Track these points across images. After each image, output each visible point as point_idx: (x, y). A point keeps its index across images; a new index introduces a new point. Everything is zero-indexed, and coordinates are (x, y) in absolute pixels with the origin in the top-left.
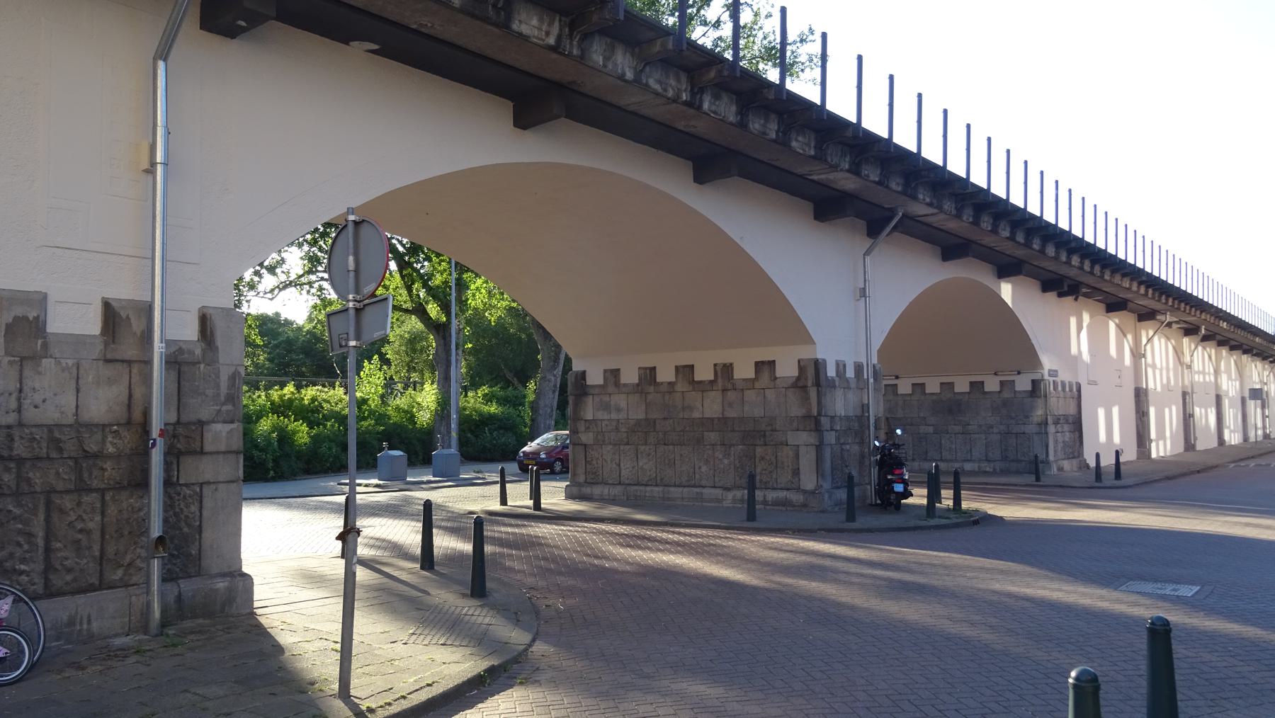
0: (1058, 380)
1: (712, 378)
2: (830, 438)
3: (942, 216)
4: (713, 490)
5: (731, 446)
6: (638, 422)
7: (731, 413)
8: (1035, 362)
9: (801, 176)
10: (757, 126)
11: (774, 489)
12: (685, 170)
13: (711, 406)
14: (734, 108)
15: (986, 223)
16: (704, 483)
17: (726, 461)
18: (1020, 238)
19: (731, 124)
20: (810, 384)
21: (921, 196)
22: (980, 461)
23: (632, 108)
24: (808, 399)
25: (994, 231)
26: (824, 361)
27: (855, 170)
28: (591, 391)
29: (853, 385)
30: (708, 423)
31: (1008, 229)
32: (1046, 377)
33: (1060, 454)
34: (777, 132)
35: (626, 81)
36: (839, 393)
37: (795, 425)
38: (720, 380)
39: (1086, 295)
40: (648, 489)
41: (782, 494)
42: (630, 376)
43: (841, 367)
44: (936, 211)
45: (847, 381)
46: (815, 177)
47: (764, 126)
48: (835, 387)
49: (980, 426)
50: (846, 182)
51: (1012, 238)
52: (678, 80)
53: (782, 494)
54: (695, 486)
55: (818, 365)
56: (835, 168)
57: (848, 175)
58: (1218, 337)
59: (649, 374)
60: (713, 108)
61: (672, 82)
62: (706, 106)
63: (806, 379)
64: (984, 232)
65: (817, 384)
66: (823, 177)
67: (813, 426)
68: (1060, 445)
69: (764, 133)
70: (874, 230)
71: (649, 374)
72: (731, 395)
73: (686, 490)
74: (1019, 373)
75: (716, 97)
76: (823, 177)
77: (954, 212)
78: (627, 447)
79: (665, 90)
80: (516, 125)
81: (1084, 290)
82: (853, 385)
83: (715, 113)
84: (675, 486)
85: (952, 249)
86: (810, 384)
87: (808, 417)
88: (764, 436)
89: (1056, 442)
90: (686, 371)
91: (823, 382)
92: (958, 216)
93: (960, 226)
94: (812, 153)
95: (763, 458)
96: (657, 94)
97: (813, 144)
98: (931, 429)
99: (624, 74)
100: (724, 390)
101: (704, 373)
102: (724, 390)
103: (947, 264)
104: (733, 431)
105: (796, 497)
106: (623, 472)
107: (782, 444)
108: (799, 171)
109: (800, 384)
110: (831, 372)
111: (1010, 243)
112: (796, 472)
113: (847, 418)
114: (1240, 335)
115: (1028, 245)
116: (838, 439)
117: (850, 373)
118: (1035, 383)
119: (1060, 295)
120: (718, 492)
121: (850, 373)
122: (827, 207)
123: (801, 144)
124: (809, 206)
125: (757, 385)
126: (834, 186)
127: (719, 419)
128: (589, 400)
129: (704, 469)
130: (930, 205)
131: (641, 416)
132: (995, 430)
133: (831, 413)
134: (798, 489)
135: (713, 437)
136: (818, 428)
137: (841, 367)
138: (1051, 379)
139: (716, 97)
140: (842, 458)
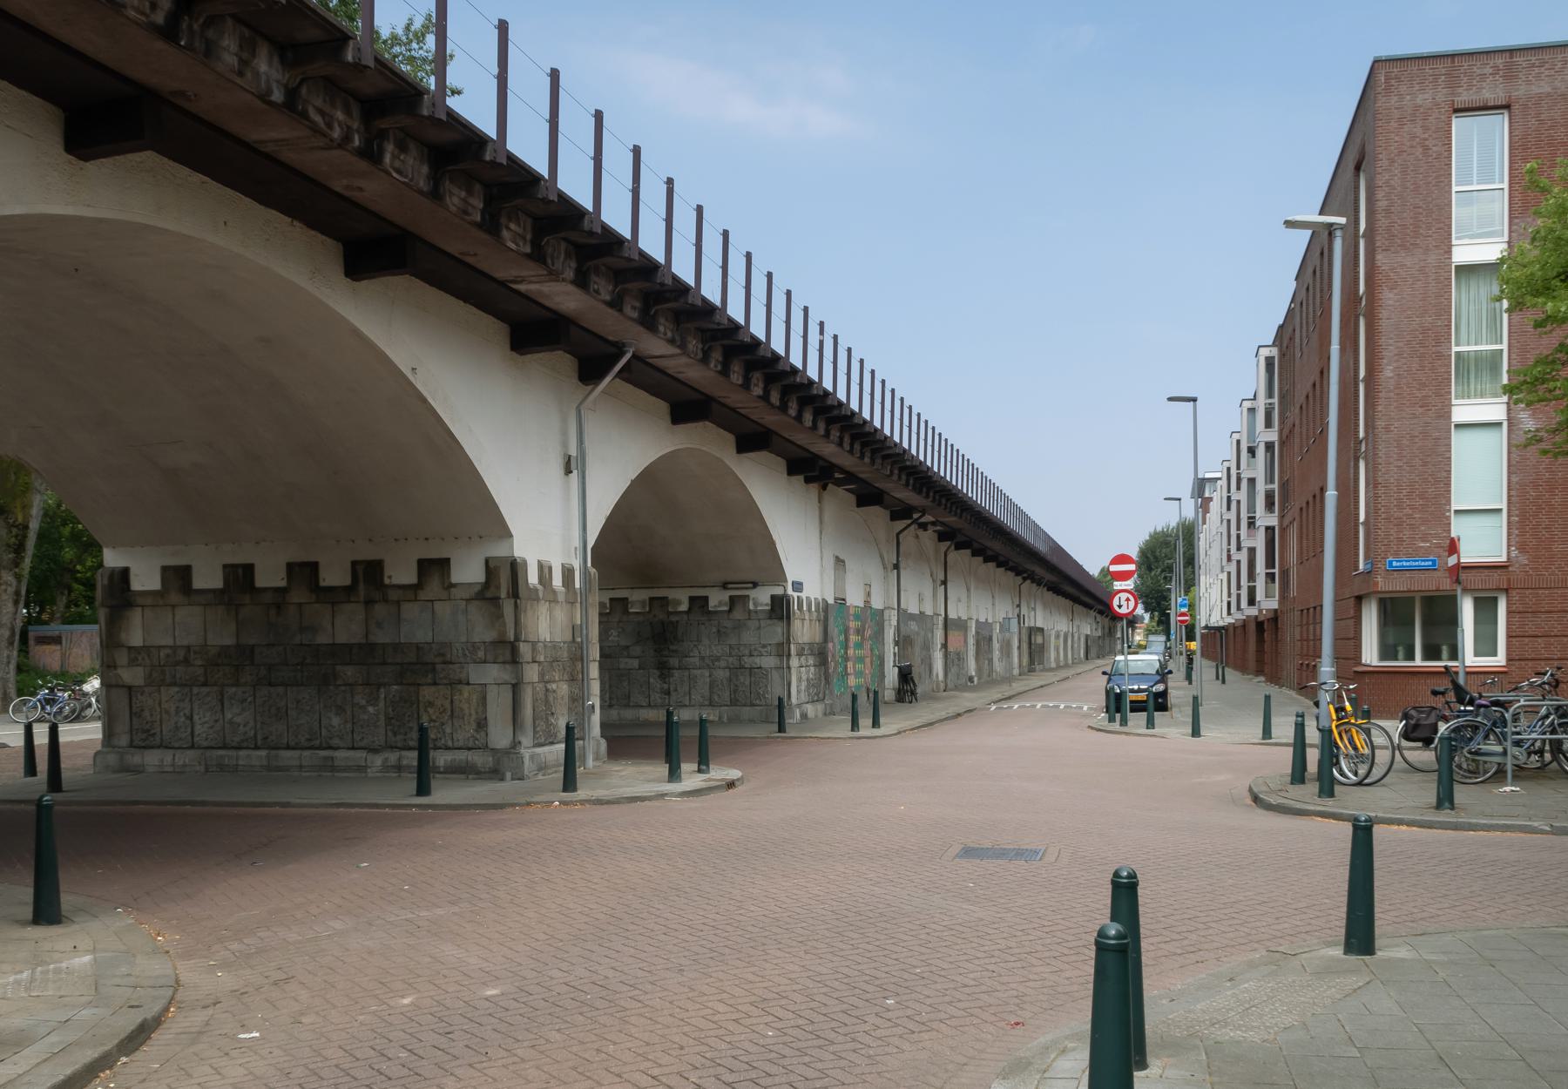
0: (803, 595)
1: (348, 582)
2: (531, 673)
3: (684, 360)
4: (351, 753)
5: (379, 686)
6: (224, 650)
7: (381, 637)
8: (778, 575)
9: (502, 284)
10: (456, 200)
11: (448, 748)
12: (328, 251)
13: (346, 627)
14: (425, 169)
15: (515, 235)
16: (335, 742)
17: (371, 709)
18: (775, 398)
19: (421, 192)
20: (503, 595)
21: (661, 329)
22: (702, 705)
23: (732, 405)
24: (500, 616)
25: (746, 385)
26: (525, 562)
27: (581, 281)
28: (140, 601)
29: (561, 598)
30: (341, 653)
31: (761, 385)
32: (790, 591)
33: (804, 697)
34: (483, 212)
35: (270, 103)
36: (543, 609)
37: (481, 654)
38: (361, 586)
39: (838, 483)
40: (242, 753)
41: (461, 756)
42: (208, 578)
43: (544, 570)
44: (678, 351)
45: (554, 592)
46: (522, 287)
47: (465, 200)
48: (538, 600)
49: (702, 658)
50: (564, 297)
51: (765, 397)
52: (348, 112)
53: (461, 756)
54: (320, 748)
55: (515, 568)
56: (554, 276)
57: (571, 288)
58: (975, 545)
59: (240, 577)
60: (397, 164)
61: (340, 115)
62: (387, 159)
63: (498, 588)
64: (451, 221)
65: (515, 594)
66: (533, 287)
67: (508, 657)
68: (804, 684)
69: (466, 212)
70: (590, 372)
71: (240, 577)
72: (380, 610)
73: (307, 753)
74: (755, 585)
75: (402, 147)
76: (533, 287)
77: (700, 355)
78: (205, 690)
79: (330, 126)
80: (347, 274)
81: (837, 475)
82: (561, 598)
83: (399, 172)
84: (288, 748)
85: (687, 408)
86: (503, 595)
87: (500, 642)
88: (434, 670)
89: (800, 680)
90: (304, 572)
91: (522, 592)
92: (705, 360)
93: (695, 373)
94: (528, 250)
95: (431, 704)
96: (316, 130)
97: (529, 237)
98: (635, 663)
99: (269, 92)
100: (369, 603)
101: (334, 575)
102: (369, 603)
103: (91, 166)
104: (384, 663)
105: (478, 758)
106: (198, 729)
107: (460, 682)
108: (500, 274)
109: (489, 594)
110: (533, 578)
111: (762, 404)
112: (482, 725)
113: (554, 646)
114: (996, 546)
115: (783, 408)
116: (542, 675)
117: (557, 581)
118: (491, 568)
119: (808, 480)
120: (360, 755)
121: (557, 581)
122: (532, 332)
123: (405, 168)
124: (663, 407)
125: (422, 595)
126: (547, 303)
127: (360, 645)
128: (136, 617)
129: (336, 721)
130: (672, 341)
131: (229, 641)
132: (723, 664)
133: (532, 638)
134: (486, 747)
135: (349, 672)
136: (514, 660)
137: (544, 570)
138: (795, 595)
139: (402, 147)
140: (547, 701)
